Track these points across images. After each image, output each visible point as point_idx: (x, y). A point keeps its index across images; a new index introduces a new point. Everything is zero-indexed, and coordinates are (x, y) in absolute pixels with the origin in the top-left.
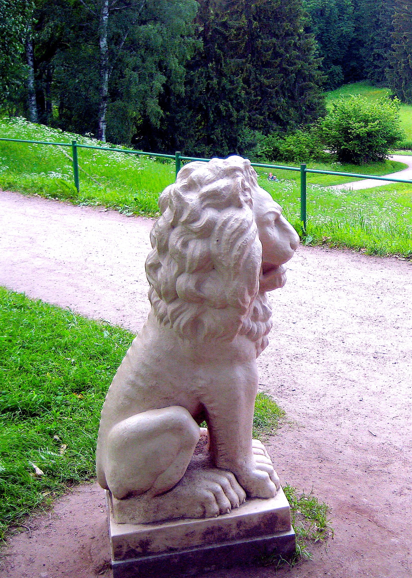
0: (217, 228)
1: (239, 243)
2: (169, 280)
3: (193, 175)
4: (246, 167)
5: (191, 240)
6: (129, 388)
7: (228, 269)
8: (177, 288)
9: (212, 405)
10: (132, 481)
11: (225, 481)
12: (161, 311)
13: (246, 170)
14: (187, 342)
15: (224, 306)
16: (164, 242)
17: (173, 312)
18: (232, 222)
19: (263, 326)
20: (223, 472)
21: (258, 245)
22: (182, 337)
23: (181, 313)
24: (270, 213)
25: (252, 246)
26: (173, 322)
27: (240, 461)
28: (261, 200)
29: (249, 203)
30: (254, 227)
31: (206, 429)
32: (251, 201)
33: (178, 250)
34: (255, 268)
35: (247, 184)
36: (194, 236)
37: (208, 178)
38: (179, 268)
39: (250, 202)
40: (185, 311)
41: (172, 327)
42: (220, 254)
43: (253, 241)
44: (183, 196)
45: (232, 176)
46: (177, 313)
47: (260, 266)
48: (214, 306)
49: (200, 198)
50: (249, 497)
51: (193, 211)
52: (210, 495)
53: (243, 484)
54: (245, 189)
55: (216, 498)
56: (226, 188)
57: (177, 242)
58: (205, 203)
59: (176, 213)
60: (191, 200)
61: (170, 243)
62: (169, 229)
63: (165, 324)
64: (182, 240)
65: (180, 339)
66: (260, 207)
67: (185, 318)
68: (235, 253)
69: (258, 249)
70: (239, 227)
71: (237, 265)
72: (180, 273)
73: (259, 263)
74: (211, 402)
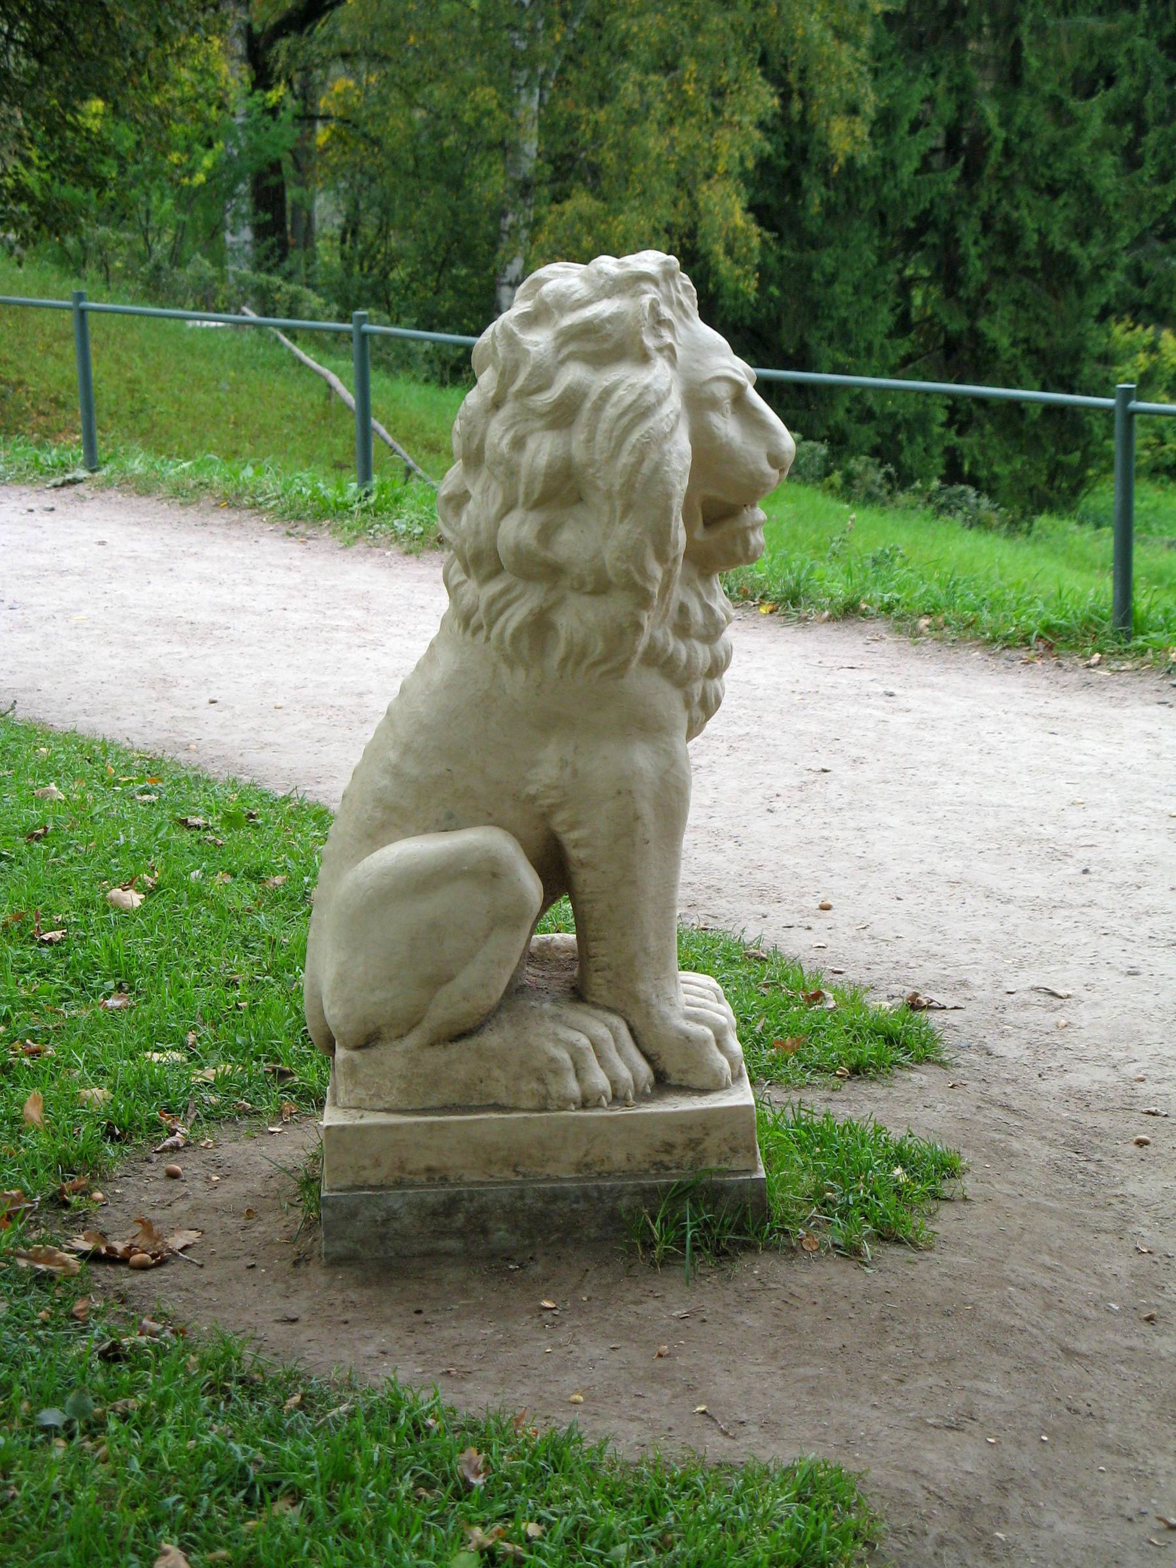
0: (588, 405)
1: (634, 437)
2: (483, 526)
3: (546, 288)
4: (668, 275)
5: (531, 432)
6: (386, 781)
7: (609, 495)
8: (499, 541)
9: (574, 835)
10: (379, 995)
11: (602, 1032)
12: (467, 600)
13: (666, 280)
14: (521, 674)
15: (601, 587)
16: (476, 441)
17: (492, 602)
18: (620, 392)
19: (703, 654)
20: (600, 1013)
21: (682, 445)
22: (511, 663)
23: (508, 605)
24: (718, 379)
25: (666, 447)
26: (491, 625)
27: (644, 988)
28: (699, 350)
29: (666, 353)
30: (674, 403)
31: (572, 937)
32: (671, 348)
33: (502, 455)
34: (668, 496)
35: (666, 312)
36: (538, 424)
37: (577, 296)
38: (505, 498)
39: (669, 351)
40: (516, 599)
41: (488, 639)
42: (591, 463)
43: (667, 436)
44: (521, 336)
45: (631, 292)
46: (500, 604)
47: (683, 494)
48: (579, 587)
49: (556, 339)
50: (662, 1084)
51: (538, 367)
52: (564, 1056)
53: (647, 1048)
54: (660, 322)
55: (575, 1064)
56: (613, 319)
57: (502, 438)
58: (565, 351)
59: (502, 374)
60: (537, 344)
61: (488, 442)
62: (487, 411)
63: (474, 633)
64: (511, 433)
65: (504, 669)
66: (695, 366)
67: (517, 615)
68: (625, 459)
69: (681, 456)
70: (635, 401)
71: (629, 486)
72: (508, 508)
73: (681, 486)
74: (573, 826)
